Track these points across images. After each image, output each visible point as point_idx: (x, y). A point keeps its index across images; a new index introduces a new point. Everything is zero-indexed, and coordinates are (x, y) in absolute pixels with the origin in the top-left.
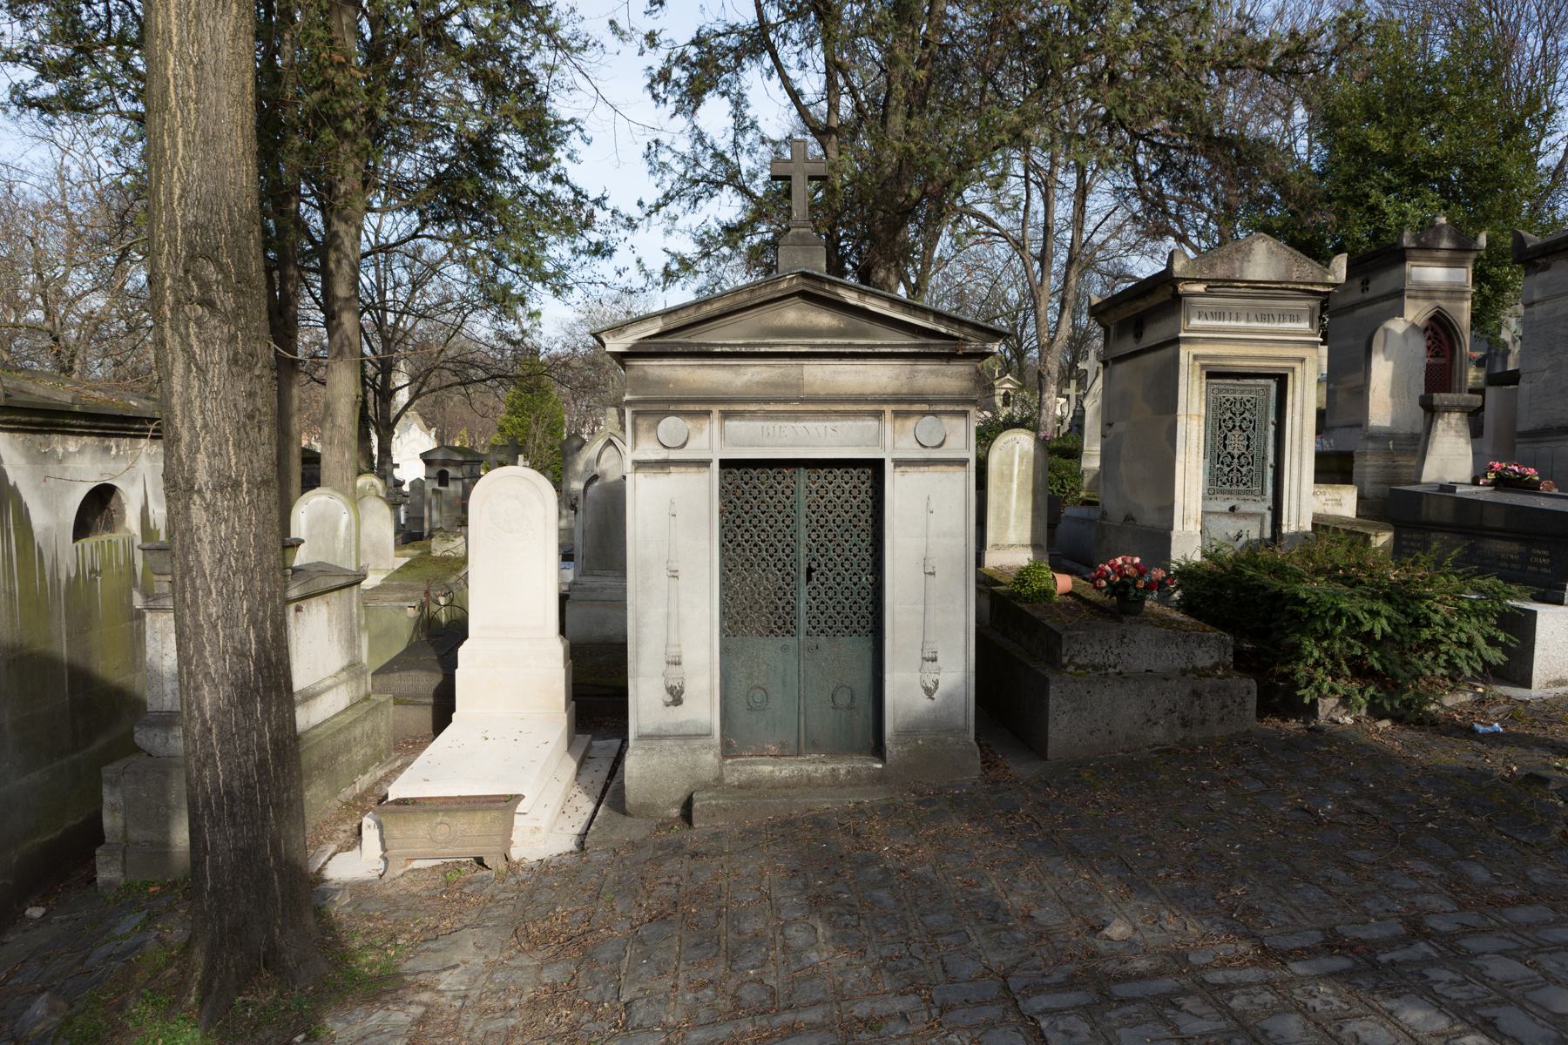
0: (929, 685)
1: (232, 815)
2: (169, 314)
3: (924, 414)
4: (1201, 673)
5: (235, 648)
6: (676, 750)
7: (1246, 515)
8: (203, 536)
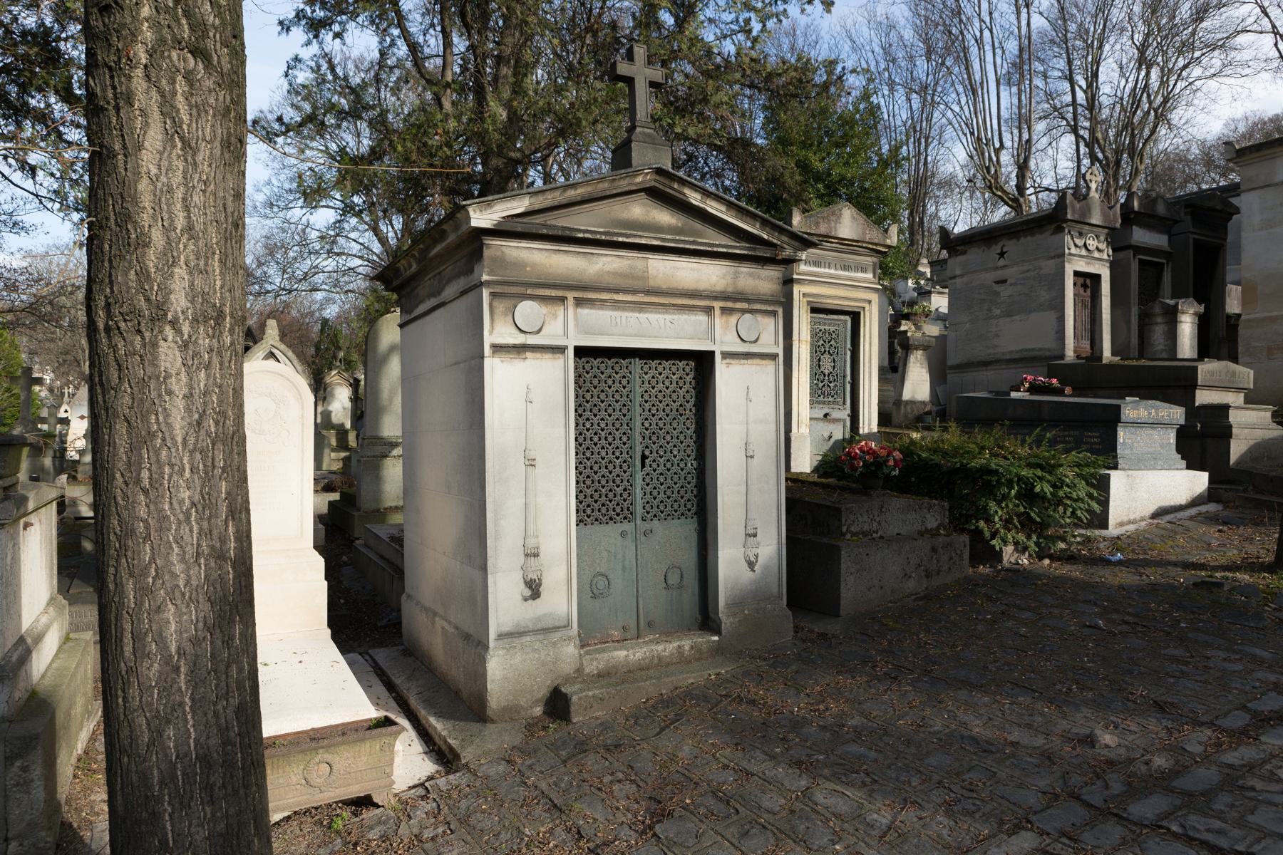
0: (752, 559)
1: (208, 787)
2: (144, 58)
3: (744, 311)
4: (934, 533)
5: (213, 548)
6: (537, 645)
7: (835, 421)
8: (175, 388)
